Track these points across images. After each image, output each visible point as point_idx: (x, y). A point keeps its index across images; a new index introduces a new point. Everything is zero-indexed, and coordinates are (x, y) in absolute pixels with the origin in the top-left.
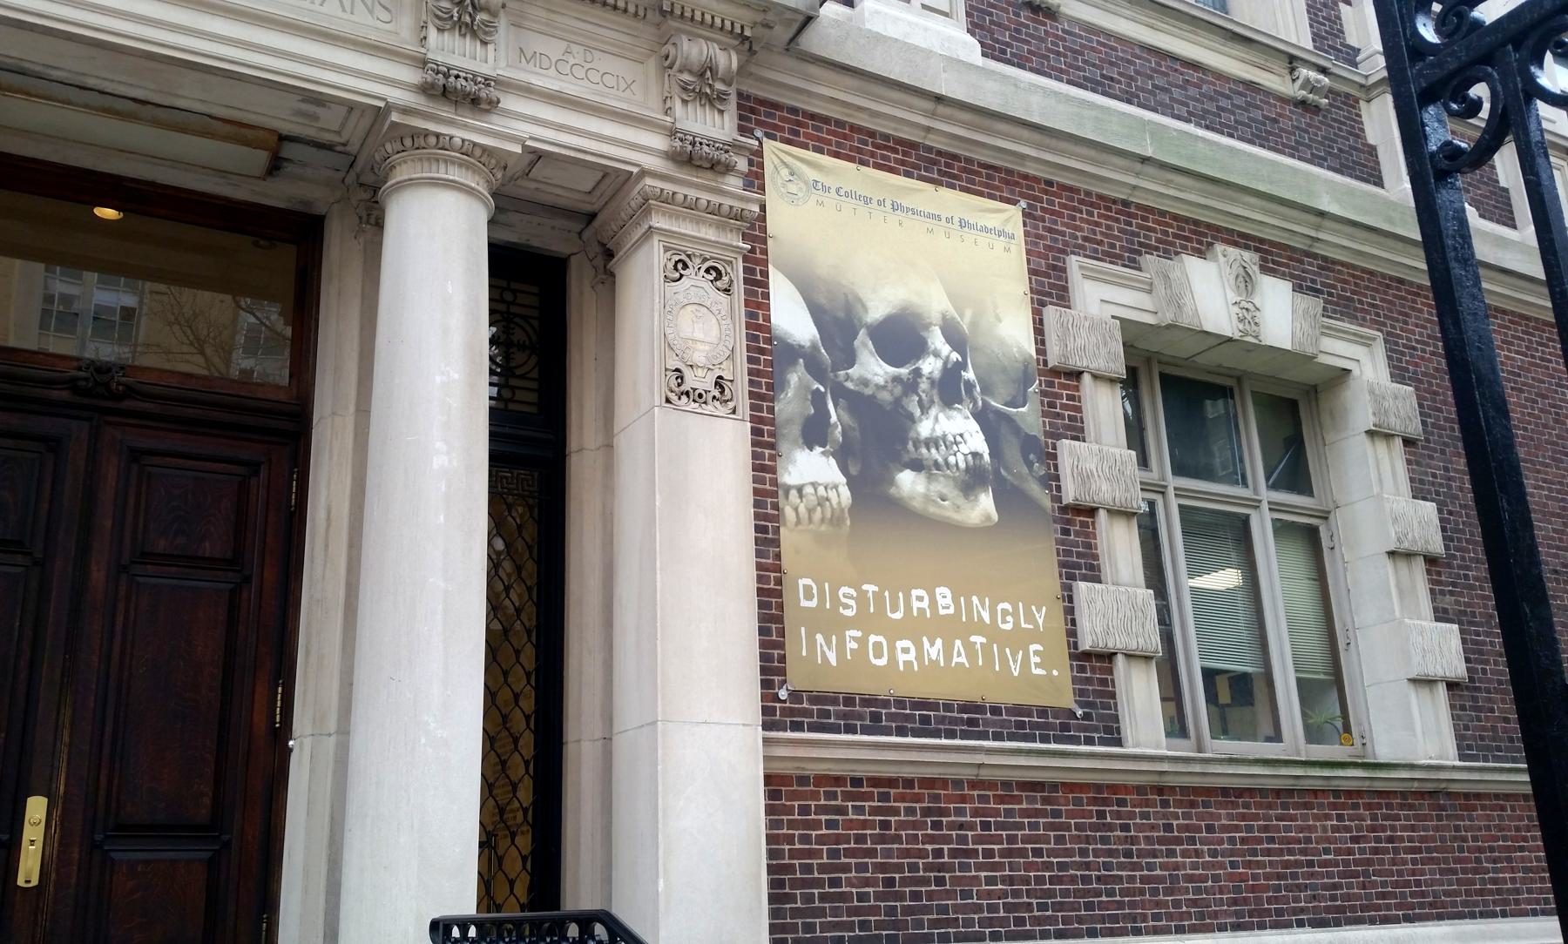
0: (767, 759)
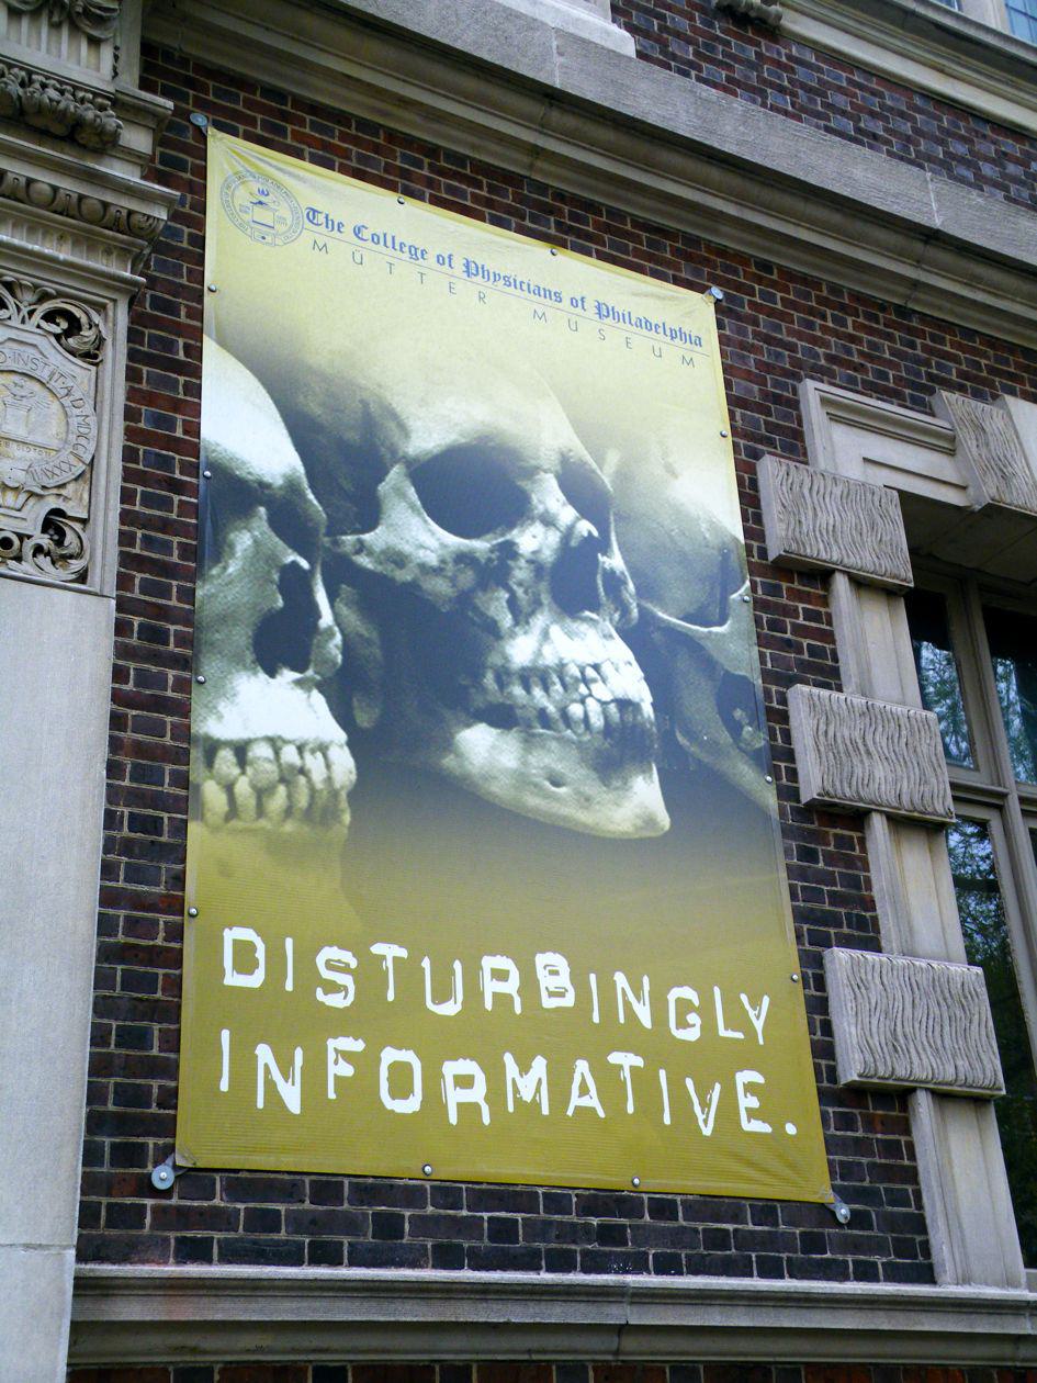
0: (84, 1287)
